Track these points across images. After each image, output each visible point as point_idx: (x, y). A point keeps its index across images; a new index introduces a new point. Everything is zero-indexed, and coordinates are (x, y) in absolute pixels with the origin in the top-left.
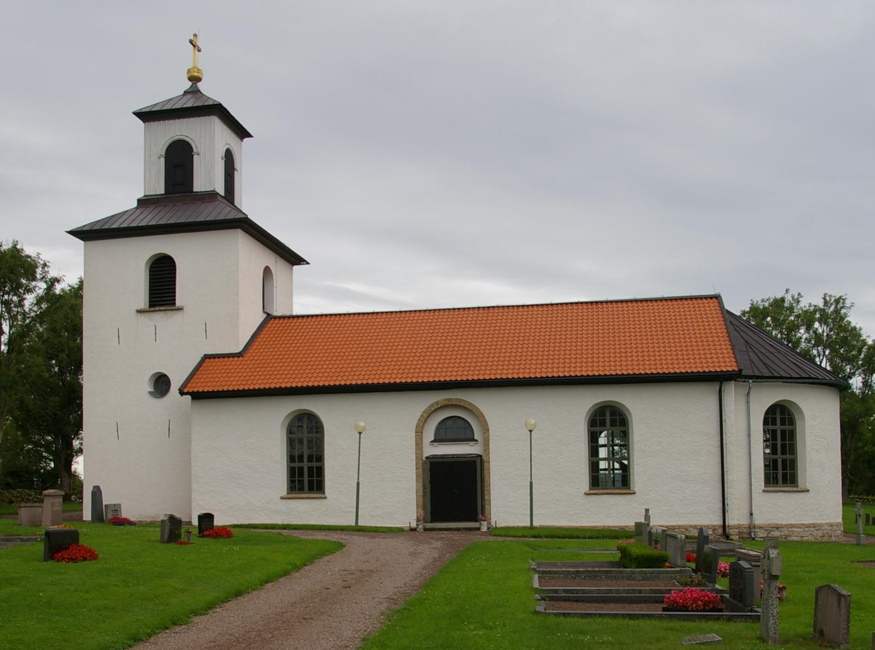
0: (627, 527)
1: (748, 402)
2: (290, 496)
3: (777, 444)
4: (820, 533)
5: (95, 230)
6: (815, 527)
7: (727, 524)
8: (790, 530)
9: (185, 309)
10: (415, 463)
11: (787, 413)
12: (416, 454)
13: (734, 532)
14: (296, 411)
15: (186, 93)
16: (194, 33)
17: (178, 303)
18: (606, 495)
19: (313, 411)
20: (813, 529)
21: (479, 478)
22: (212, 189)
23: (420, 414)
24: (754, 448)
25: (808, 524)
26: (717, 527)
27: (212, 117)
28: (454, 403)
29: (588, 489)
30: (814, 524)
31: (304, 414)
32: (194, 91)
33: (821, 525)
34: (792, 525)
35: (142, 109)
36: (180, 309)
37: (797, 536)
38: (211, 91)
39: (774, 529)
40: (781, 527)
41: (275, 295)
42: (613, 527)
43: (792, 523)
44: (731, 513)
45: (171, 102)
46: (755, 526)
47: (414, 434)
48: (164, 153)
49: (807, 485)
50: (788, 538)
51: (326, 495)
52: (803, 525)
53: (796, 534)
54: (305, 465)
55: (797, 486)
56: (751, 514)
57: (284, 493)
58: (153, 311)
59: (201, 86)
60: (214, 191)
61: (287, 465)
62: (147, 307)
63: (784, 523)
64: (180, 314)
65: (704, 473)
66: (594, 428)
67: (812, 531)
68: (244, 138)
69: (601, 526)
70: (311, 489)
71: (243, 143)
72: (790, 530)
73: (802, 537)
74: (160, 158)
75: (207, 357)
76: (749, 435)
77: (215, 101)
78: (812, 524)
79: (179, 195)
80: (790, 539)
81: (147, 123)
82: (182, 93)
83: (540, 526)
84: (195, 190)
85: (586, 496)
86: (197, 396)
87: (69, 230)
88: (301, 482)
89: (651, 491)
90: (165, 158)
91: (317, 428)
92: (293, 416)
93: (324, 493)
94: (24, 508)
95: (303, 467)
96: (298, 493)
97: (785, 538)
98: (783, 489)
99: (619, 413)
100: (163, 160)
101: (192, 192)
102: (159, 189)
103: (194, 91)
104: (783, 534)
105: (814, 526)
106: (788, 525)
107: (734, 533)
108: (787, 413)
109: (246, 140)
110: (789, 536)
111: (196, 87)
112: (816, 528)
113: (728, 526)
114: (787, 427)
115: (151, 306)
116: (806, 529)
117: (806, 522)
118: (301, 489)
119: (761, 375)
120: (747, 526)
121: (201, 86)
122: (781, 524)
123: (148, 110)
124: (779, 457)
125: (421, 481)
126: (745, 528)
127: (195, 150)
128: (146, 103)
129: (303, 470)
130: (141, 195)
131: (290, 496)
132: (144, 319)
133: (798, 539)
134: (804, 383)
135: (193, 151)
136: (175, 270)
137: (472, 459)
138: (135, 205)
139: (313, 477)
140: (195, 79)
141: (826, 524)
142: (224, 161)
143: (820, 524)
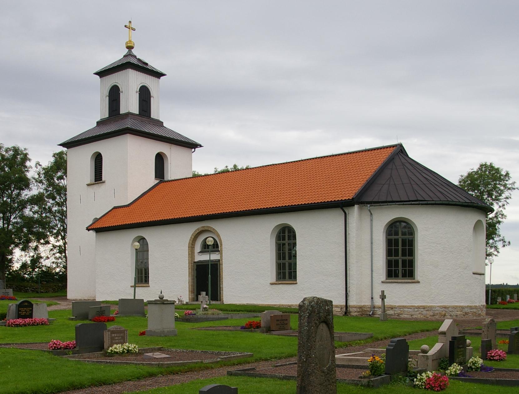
0: (292, 305)
1: (372, 220)
2: (277, 282)
4: (431, 313)
6: (424, 308)
7: (348, 304)
8: (402, 309)
10: (188, 265)
11: (292, 232)
12: (189, 260)
13: (353, 310)
16: (129, 21)
17: (103, 179)
18: (281, 285)
20: (422, 310)
21: (219, 274)
22: (128, 111)
23: (190, 237)
24: (376, 252)
25: (417, 306)
26: (343, 307)
27: (127, 69)
28: (206, 229)
29: (385, 278)
30: (424, 306)
33: (431, 307)
34: (403, 306)
37: (408, 315)
38: (140, 53)
39: (390, 309)
40: (394, 308)
41: (169, 168)
42: (285, 305)
43: (403, 305)
44: (352, 297)
46: (375, 307)
47: (188, 248)
48: (108, 94)
49: (418, 278)
50: (401, 316)
51: (150, 285)
52: (413, 306)
53: (406, 313)
54: (400, 258)
55: (414, 279)
56: (372, 298)
57: (274, 280)
58: (98, 183)
61: (276, 262)
62: (93, 182)
63: (397, 305)
64: (103, 184)
65: (337, 270)
66: (403, 236)
67: (422, 311)
68: (160, 77)
69: (278, 305)
70: (404, 276)
71: (160, 80)
72: (402, 309)
73: (412, 315)
75: (115, 208)
76: (372, 243)
78: (421, 306)
79: (112, 117)
80: (402, 316)
82: (122, 57)
83: (247, 304)
84: (121, 113)
85: (270, 285)
86: (99, 231)
87: (59, 144)
88: (284, 274)
89: (306, 282)
90: (109, 97)
92: (277, 231)
93: (296, 280)
94: (138, 288)
95: (285, 263)
96: (141, 284)
97: (398, 316)
98: (403, 281)
99: (293, 231)
100: (108, 98)
101: (120, 114)
104: (396, 313)
105: (424, 308)
106: (400, 306)
107: (353, 311)
108: (292, 232)
109: (162, 78)
110: (401, 314)
112: (426, 309)
113: (349, 306)
115: (95, 181)
116: (416, 310)
117: (416, 305)
118: (284, 278)
119: (424, 200)
120: (369, 306)
121: (134, 51)
122: (394, 306)
123: (103, 70)
124: (287, 261)
125: (191, 276)
126: (368, 307)
127: (121, 90)
128: (100, 67)
129: (285, 264)
130: (98, 119)
131: (277, 282)
132: (91, 189)
133: (408, 316)
134: (419, 204)
136: (102, 159)
137: (216, 263)
138: (95, 125)
140: (130, 48)
141: (438, 306)
143: (431, 306)
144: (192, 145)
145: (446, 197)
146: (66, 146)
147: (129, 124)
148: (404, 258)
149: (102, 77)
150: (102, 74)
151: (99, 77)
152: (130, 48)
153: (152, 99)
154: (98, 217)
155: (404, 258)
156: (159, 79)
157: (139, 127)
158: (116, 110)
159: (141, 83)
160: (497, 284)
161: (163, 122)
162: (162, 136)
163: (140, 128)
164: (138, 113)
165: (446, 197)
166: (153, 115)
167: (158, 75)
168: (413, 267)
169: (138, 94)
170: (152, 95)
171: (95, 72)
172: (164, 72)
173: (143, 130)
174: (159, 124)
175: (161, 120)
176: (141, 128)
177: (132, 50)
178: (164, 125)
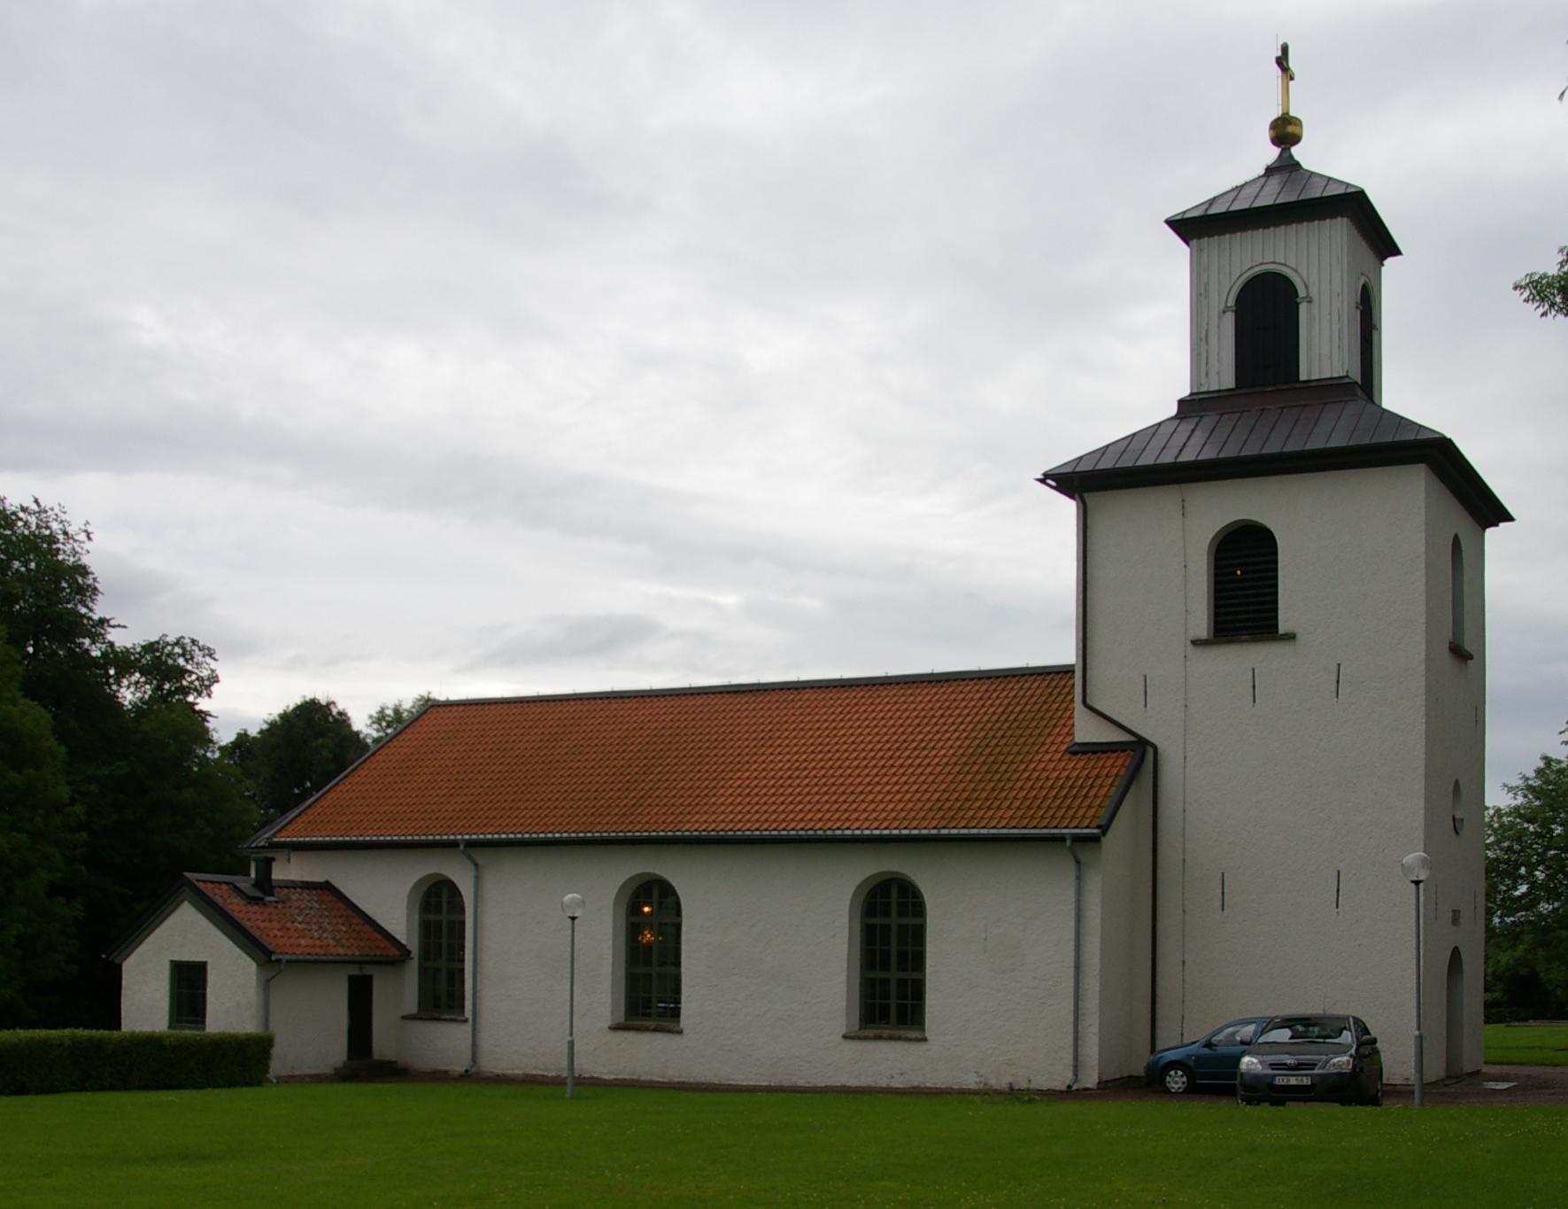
3: (889, 903)
5: (1225, 459)
9: (1298, 636)
14: (873, 876)
15: (1270, 171)
17: (1283, 627)
19: (908, 874)
31: (892, 879)
32: (1286, 167)
35: (1184, 212)
36: (1290, 637)
45: (1244, 192)
48: (1231, 302)
51: (927, 1035)
54: (894, 920)
59: (1297, 152)
60: (1347, 377)
74: (1224, 312)
77: (1348, 185)
81: (1194, 242)
91: (914, 905)
100: (1230, 320)
101: (1297, 380)
102: (1225, 378)
103: (1286, 167)
111: (1291, 157)
114: (432, 917)
115: (1215, 636)
123: (1179, 217)
127: (1302, 293)
135: (1297, 296)
136: (1275, 553)
139: (907, 1004)
142: (1359, 312)
148: (884, 921)
152: (1285, 132)
155: (884, 921)
171: (1169, 214)
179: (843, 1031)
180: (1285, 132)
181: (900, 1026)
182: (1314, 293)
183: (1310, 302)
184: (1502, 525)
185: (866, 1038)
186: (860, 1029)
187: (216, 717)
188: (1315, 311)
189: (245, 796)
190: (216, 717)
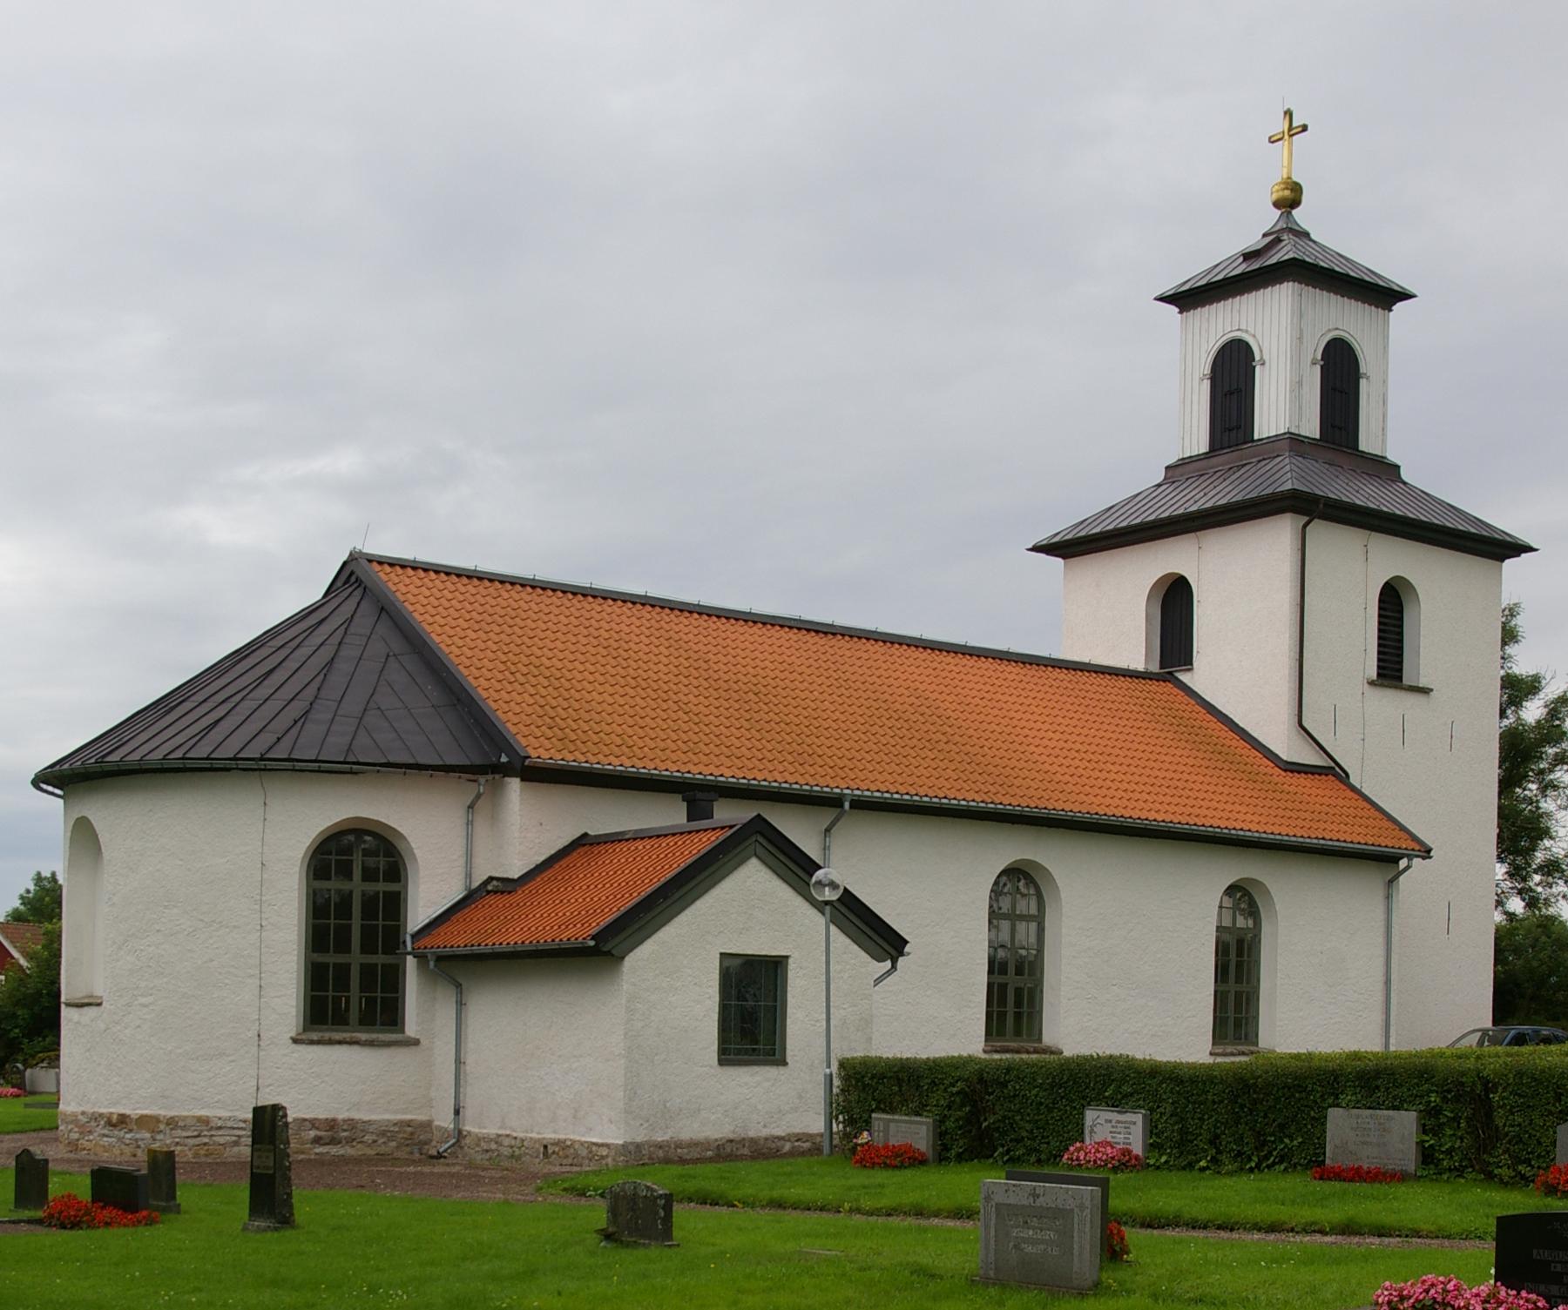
48: (1207, 370)
54: (356, 958)
55: (403, 1031)
70: (367, 1021)
71: (1391, 313)
100: (1207, 384)
101: (1253, 441)
109: (1399, 307)
123: (1203, 282)
127: (1257, 357)
144: (1500, 548)
145: (197, 738)
146: (1056, 553)
147: (1286, 476)
148: (341, 959)
149: (1188, 311)
150: (1186, 299)
151: (1177, 310)
152: (1290, 199)
153: (1363, 383)
154: (1354, 780)
155: (341, 959)
156: (1390, 310)
157: (1321, 487)
158: (1239, 427)
159: (1329, 330)
160: (1116, 1053)
161: (1398, 467)
162: (1394, 515)
163: (1324, 489)
164: (1318, 437)
165: (197, 738)
166: (1366, 444)
167: (1384, 296)
168: (397, 992)
169: (1318, 367)
170: (1362, 370)
171: (1158, 293)
172: (1409, 286)
173: (1348, 500)
174: (1386, 471)
175: (1392, 456)
176: (1314, 488)
177: (1294, 212)
178: (1404, 475)
179: (293, 1034)
180: (1290, 199)
181: (316, 1027)
182: (1266, 357)
183: (1263, 364)
184: (1523, 555)
185: (312, 1042)
186: (305, 1030)
187: (878, 981)
188: (1267, 372)
189: (665, 1215)
190: (878, 981)
